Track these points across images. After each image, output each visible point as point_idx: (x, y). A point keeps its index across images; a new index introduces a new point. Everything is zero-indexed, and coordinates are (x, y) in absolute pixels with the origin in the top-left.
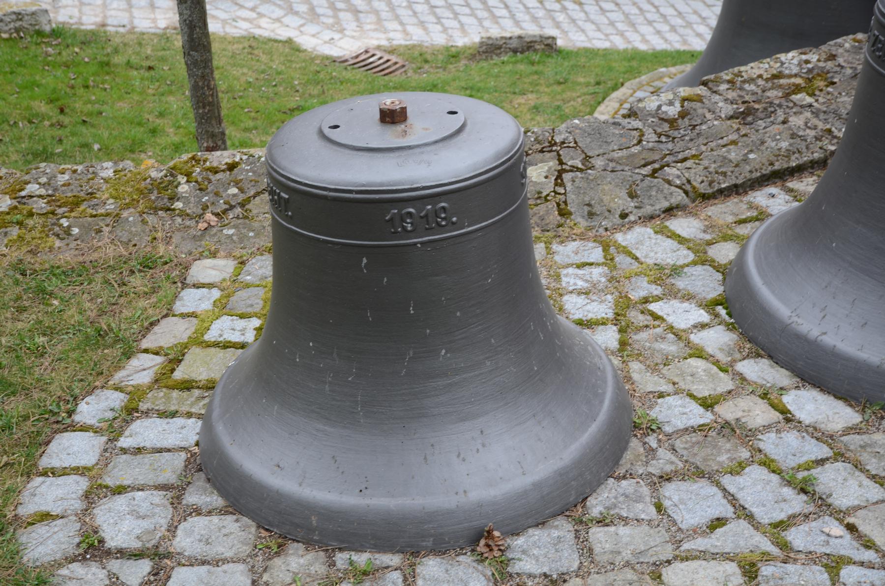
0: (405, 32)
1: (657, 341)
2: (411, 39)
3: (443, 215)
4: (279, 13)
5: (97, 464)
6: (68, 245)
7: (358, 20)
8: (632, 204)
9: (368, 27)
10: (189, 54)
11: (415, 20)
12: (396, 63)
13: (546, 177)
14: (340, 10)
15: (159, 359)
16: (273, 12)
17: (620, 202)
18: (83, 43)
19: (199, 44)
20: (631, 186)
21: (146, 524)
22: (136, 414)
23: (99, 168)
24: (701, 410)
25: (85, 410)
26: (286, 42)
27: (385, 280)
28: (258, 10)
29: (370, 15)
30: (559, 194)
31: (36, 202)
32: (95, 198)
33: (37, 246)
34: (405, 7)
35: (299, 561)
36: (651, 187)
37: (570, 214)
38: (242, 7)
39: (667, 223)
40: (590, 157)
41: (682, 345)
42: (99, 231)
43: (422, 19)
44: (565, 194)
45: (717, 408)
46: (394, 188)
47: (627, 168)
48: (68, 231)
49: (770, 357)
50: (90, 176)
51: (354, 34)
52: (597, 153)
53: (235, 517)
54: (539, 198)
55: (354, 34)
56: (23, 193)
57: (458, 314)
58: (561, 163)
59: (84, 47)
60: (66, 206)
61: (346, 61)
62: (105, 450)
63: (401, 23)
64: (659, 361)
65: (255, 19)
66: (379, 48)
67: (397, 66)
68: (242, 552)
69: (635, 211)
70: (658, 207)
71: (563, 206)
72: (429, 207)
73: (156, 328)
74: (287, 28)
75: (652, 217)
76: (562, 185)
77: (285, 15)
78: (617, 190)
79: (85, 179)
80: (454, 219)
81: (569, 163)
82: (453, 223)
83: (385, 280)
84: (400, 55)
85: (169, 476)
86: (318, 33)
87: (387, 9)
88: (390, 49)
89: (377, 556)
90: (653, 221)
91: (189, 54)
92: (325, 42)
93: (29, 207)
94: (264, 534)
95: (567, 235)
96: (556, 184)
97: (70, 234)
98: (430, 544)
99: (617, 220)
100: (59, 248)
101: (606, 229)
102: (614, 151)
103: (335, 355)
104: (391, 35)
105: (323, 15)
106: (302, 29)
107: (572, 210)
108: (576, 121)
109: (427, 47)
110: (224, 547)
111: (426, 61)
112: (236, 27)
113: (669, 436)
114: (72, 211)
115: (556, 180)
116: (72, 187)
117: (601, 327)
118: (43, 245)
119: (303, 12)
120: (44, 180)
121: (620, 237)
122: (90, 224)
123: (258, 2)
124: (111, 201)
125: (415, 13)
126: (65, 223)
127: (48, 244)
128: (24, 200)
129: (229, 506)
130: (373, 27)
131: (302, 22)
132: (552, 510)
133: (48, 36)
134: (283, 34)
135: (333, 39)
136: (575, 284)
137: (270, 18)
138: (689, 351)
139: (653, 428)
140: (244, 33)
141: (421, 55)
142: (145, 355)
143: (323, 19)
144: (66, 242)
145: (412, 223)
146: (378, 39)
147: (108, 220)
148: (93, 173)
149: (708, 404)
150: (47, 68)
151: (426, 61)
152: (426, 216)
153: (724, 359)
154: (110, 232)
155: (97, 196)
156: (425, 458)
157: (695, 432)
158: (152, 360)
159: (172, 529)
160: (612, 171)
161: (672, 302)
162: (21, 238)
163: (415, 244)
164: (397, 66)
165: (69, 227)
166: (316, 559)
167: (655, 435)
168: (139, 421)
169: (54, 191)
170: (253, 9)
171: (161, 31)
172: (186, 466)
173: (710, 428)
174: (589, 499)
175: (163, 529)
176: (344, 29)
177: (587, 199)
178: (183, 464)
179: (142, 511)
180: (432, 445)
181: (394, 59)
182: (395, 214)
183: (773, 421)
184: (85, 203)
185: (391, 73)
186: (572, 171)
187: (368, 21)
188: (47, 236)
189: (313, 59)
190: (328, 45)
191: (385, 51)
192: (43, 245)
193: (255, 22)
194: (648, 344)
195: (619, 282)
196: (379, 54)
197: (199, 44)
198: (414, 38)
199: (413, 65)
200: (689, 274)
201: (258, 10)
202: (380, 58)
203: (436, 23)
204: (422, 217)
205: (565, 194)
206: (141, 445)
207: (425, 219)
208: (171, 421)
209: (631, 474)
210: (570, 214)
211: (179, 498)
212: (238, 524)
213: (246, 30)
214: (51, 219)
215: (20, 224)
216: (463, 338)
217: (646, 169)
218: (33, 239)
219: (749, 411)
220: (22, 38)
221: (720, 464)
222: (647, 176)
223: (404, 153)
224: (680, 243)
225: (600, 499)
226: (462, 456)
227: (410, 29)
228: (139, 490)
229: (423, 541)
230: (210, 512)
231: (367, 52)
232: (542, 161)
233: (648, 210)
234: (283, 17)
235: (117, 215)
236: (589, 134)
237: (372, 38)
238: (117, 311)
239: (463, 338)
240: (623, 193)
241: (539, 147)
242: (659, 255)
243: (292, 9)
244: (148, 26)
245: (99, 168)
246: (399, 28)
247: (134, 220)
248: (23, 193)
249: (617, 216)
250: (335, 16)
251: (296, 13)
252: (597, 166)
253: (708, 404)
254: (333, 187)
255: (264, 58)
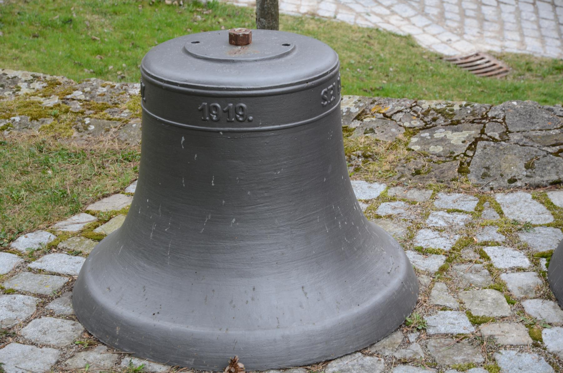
0: (522, 43)
1: (471, 272)
2: (525, 49)
3: (240, 113)
4: (410, 12)
5: (7, 274)
6: (82, 136)
7: (481, 27)
8: (525, 173)
9: (489, 34)
10: (259, 21)
11: (537, 34)
12: (501, 68)
13: (463, 142)
14: (468, 17)
15: (93, 218)
16: (406, 11)
17: (515, 170)
18: (229, 16)
19: (268, 13)
20: (532, 159)
21: (12, 315)
22: (54, 250)
23: (131, 86)
24: (469, 324)
25: (21, 241)
26: (405, 37)
27: (196, 156)
28: (393, 8)
29: (494, 24)
30: (468, 156)
31: (75, 104)
32: (117, 107)
33: (60, 134)
34: (532, 22)
35: (100, 356)
36: (549, 163)
37: (468, 172)
38: (380, 4)
39: (549, 194)
40: (510, 132)
41: (490, 278)
42: (108, 130)
43: (544, 33)
44: (472, 157)
45: (482, 326)
46: (206, 86)
47: (536, 145)
48: (86, 128)
49: (557, 300)
50: (122, 91)
51: (473, 38)
52: (518, 130)
53: (73, 322)
54: (450, 157)
55: (473, 38)
56: (69, 97)
57: (249, 193)
58: (482, 132)
59: (228, 19)
60: (94, 110)
61: (455, 60)
62: (18, 267)
63: (522, 35)
64: (462, 287)
65: (386, 15)
66: (489, 53)
67: (501, 70)
68: (63, 343)
69: (524, 179)
70: (546, 179)
71: (465, 165)
72: (231, 105)
73: (105, 200)
74: (413, 27)
75: (538, 186)
76: (474, 150)
77: (415, 15)
78: (518, 160)
79: (117, 93)
80: (251, 118)
81: (488, 134)
82: (249, 121)
83: (196, 156)
84: (506, 61)
85: (47, 290)
86: (439, 34)
87: (515, 21)
88: (499, 55)
89: (152, 364)
90: (538, 190)
91: (259, 21)
92: (442, 42)
93: (68, 107)
94: (86, 335)
95: (456, 187)
96: (468, 149)
97: (87, 129)
98: (191, 363)
99: (504, 183)
100: (75, 137)
101: (492, 189)
102: (534, 130)
103: (160, 210)
104: (507, 44)
105: (450, 19)
106: (426, 29)
107: (471, 170)
108: (515, 103)
109: (536, 58)
110: (53, 338)
111: (529, 70)
112: (366, 20)
113: (429, 336)
114: (96, 113)
115: (471, 145)
116: (105, 97)
117: (434, 255)
118: (64, 134)
119: (433, 15)
120: (88, 89)
121: (499, 197)
122: (104, 125)
123: (396, 2)
124: (127, 111)
125: (540, 27)
126: (87, 121)
127: (68, 134)
128: (68, 101)
129: (75, 315)
130: (493, 35)
131: (428, 22)
132: (295, 360)
133: (203, 7)
134: (406, 29)
135: (450, 40)
136: (436, 223)
137: (401, 16)
138: (492, 284)
139: (422, 328)
140: (371, 25)
141: (527, 64)
142: (86, 214)
143: (449, 23)
144: (81, 134)
145: (216, 115)
146: (492, 45)
147: (119, 124)
148: (125, 90)
149: (476, 321)
150: (189, 30)
151: (529, 70)
152: (228, 111)
153: (517, 294)
154: (115, 132)
155: (120, 106)
156: (206, 299)
157: (452, 338)
158: (89, 218)
159: (27, 321)
160: (523, 145)
161: (506, 249)
162: (52, 126)
163: (218, 132)
164: (501, 70)
165: (89, 124)
166: (110, 357)
167: (418, 333)
168: (53, 254)
169: (91, 98)
170: (388, 8)
171: (300, 15)
172: (64, 286)
173: (465, 337)
174: (332, 362)
175: (21, 320)
176: (464, 33)
177: (488, 164)
178: (63, 284)
179: (15, 307)
180: (213, 291)
181: (500, 64)
182: (205, 105)
183: (522, 343)
184: (109, 109)
185: (492, 75)
186: (487, 140)
187: (491, 29)
188: (71, 128)
189: (422, 54)
190: (443, 45)
191: (494, 56)
192: (64, 134)
193: (386, 18)
194: (462, 273)
195: (473, 227)
196: (487, 58)
197: (268, 13)
198: (528, 49)
199: (515, 72)
200: (537, 232)
201: (393, 8)
202: (488, 62)
203: (557, 39)
204: (224, 112)
205: (472, 157)
206: (43, 268)
207: (226, 114)
208: (73, 257)
209: (378, 354)
210: (468, 172)
211: (44, 303)
212: (73, 327)
213: (375, 24)
214: (80, 117)
215: (56, 116)
216: (251, 213)
217: (554, 148)
218: (60, 128)
219: (508, 333)
220: (180, 5)
221: (454, 362)
222: (551, 153)
223: (232, 65)
224: (549, 209)
225: (341, 363)
226: (234, 303)
227: (528, 40)
228: (22, 294)
229: (187, 360)
230: (59, 316)
231: (477, 55)
232: (468, 129)
233: (537, 179)
234: (412, 17)
235: (127, 122)
236: (520, 114)
237: (487, 44)
238: (87, 185)
239: (251, 213)
240: (522, 165)
241: (472, 118)
242: (523, 214)
243: (423, 11)
244: (291, 9)
245: (131, 86)
246: (518, 38)
247: (136, 126)
248: (69, 97)
249: (506, 180)
250: (462, 22)
251: (426, 15)
252: (512, 140)
253: (476, 321)
254: (166, 79)
255: (376, 47)
